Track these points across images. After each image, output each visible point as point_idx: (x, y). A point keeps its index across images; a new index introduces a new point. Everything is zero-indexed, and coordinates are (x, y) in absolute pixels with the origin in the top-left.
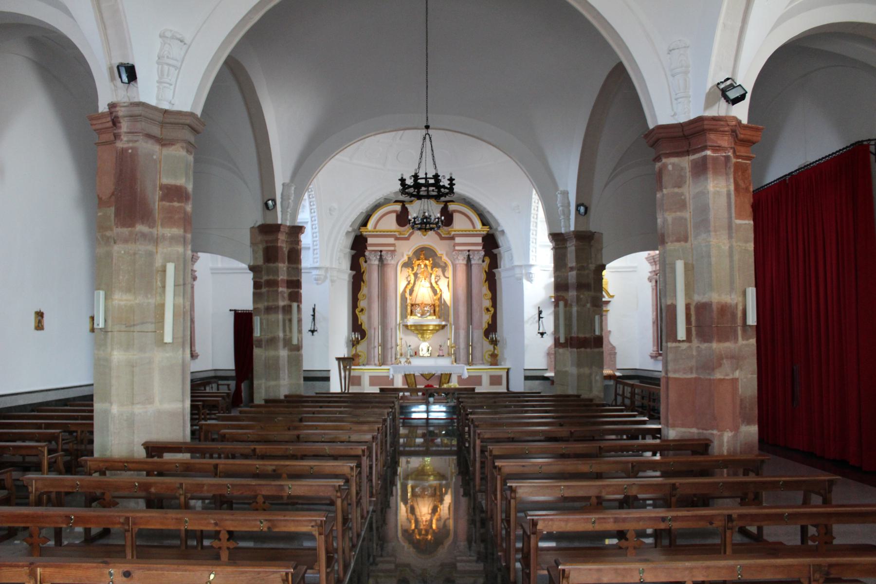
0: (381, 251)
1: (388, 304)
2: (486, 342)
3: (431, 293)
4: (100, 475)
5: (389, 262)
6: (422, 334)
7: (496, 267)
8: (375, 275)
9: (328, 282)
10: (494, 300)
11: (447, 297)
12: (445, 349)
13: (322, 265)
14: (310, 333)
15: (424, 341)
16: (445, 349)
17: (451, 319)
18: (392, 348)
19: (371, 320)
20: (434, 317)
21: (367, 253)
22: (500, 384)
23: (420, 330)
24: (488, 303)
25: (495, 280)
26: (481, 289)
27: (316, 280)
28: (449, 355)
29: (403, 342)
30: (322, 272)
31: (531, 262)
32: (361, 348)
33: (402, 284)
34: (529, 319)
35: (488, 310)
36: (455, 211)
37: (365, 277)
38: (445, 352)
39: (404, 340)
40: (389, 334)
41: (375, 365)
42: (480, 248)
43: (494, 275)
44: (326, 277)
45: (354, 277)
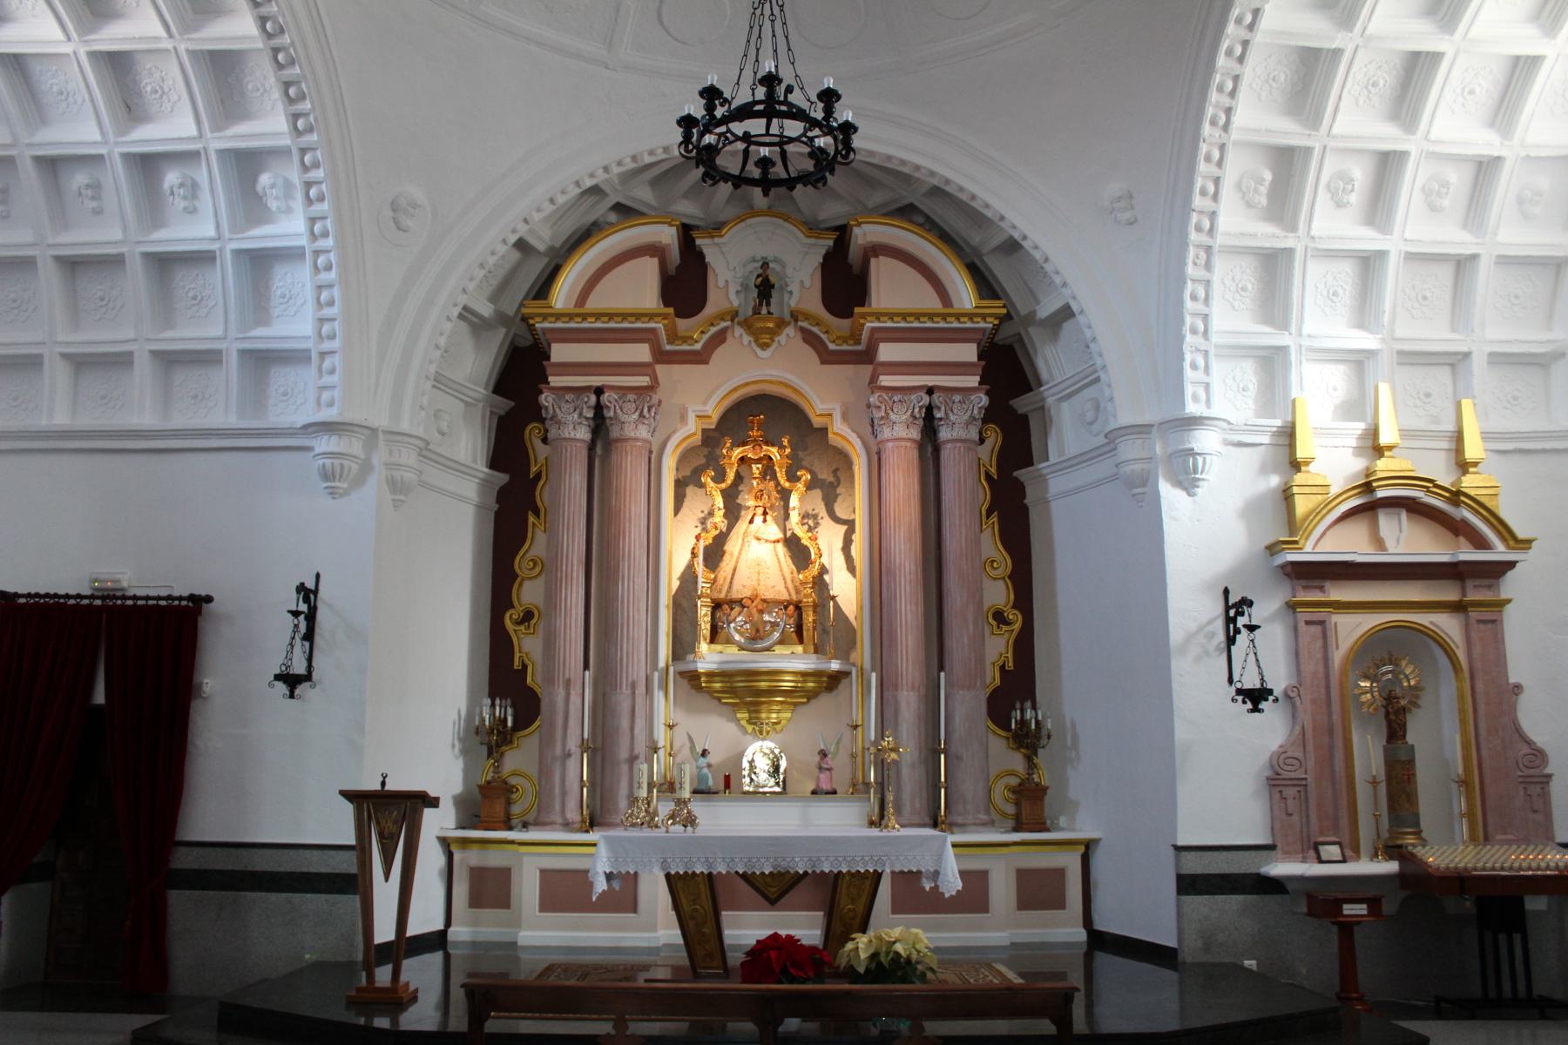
0: (599, 391)
1: (623, 588)
2: (998, 744)
3: (788, 565)
4: (581, 878)
5: (630, 432)
6: (754, 709)
7: (1028, 461)
8: (575, 480)
9: (373, 488)
10: (1022, 580)
11: (846, 589)
12: (840, 762)
13: (349, 417)
14: (281, 687)
15: (760, 734)
16: (840, 762)
17: (863, 652)
18: (633, 759)
19: (559, 653)
20: (800, 649)
21: (546, 399)
22: (1059, 903)
23: (744, 693)
24: (998, 594)
25: (1024, 512)
26: (971, 537)
27: (327, 475)
28: (858, 788)
29: (680, 739)
30: (355, 446)
31: (1192, 408)
32: (519, 759)
33: (680, 545)
34: (1190, 637)
35: (999, 617)
36: (877, 250)
37: (543, 496)
38: (841, 779)
39: (675, 730)
40: (625, 706)
41: (567, 826)
42: (973, 381)
43: (1020, 490)
44: (366, 468)
45: (503, 495)
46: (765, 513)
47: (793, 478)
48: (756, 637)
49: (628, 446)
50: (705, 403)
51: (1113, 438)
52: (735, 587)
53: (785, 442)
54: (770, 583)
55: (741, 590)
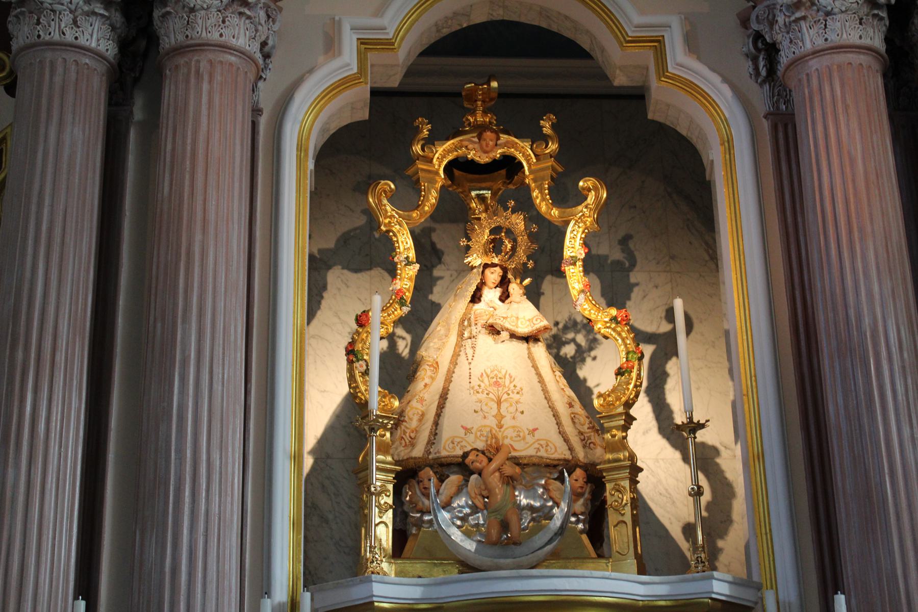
5: (207, 28)
46: (504, 283)
47: (566, 195)
48: (505, 538)
49: (203, 60)
50: (379, 12)
51: (677, 480)
52: (448, 429)
53: (547, 128)
54: (525, 422)
55: (460, 434)
